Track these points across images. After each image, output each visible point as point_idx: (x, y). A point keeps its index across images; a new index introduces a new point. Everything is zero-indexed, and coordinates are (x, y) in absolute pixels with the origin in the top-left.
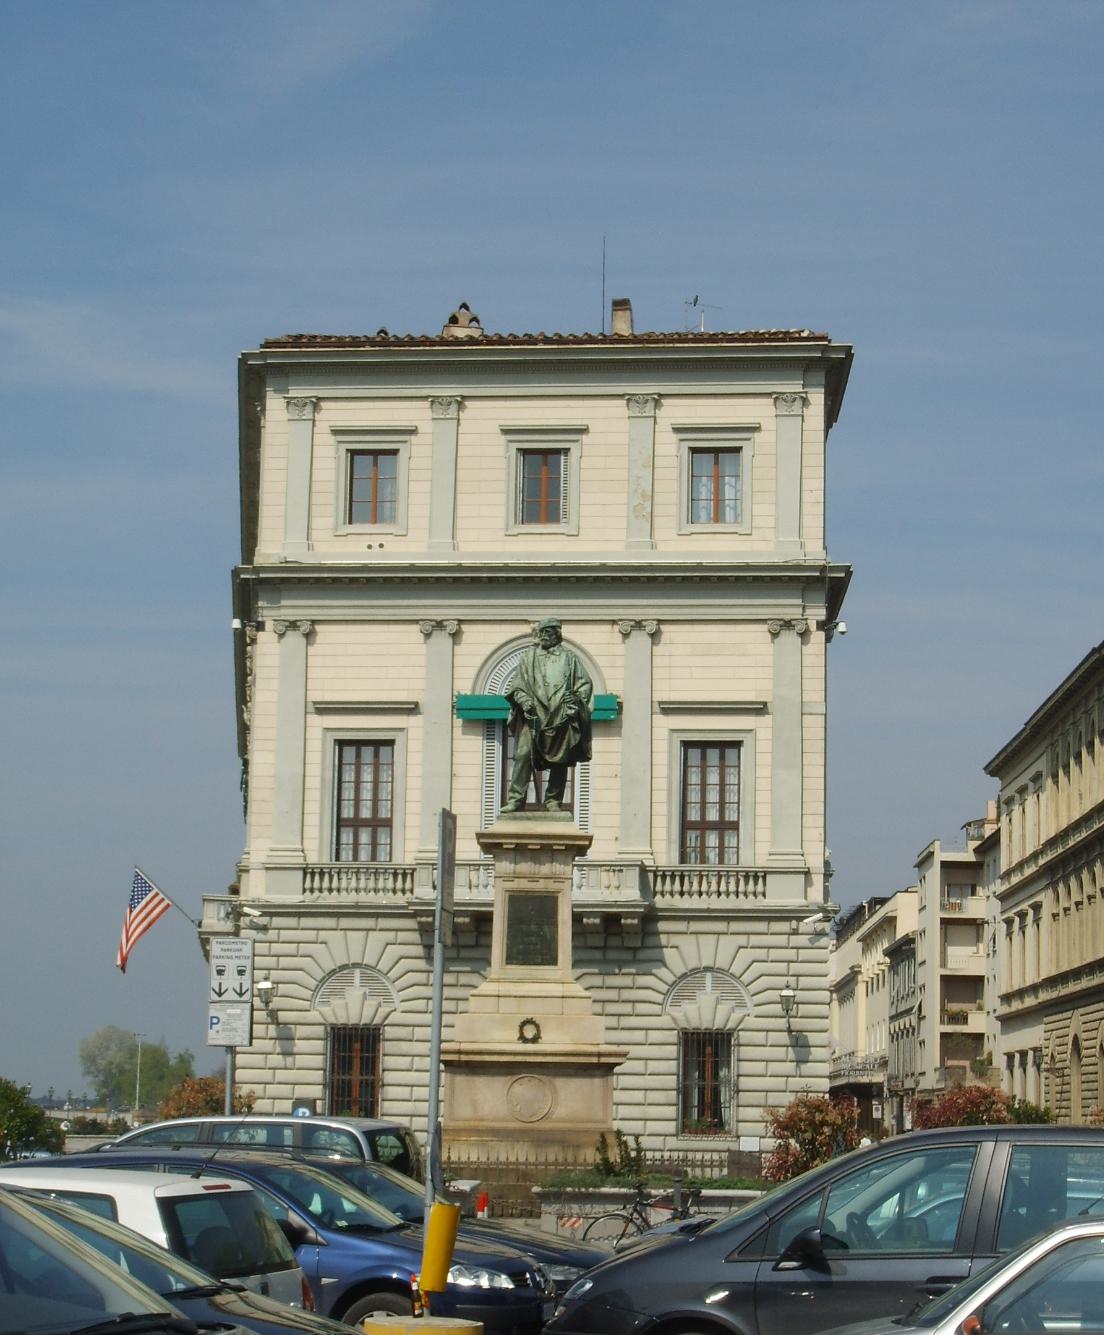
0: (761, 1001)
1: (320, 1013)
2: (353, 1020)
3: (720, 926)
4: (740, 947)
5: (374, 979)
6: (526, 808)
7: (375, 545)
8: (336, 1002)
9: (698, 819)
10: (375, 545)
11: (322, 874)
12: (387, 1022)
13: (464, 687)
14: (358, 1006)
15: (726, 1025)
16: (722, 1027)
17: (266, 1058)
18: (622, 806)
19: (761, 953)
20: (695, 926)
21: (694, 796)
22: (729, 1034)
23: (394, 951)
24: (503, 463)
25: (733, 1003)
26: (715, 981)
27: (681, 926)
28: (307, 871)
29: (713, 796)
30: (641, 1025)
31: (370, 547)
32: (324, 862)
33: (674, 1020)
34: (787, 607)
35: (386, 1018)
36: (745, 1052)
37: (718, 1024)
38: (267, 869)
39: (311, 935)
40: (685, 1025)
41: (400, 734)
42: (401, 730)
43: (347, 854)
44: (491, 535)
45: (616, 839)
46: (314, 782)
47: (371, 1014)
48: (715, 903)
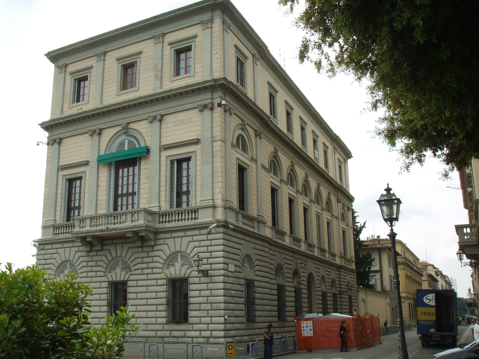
2: (178, 276)
3: (182, 234)
4: (190, 242)
10: (80, 109)
16: (183, 276)
18: (151, 187)
19: (197, 244)
20: (174, 235)
25: (188, 266)
27: (168, 235)
34: (205, 98)
37: (182, 275)
40: (170, 277)
42: (84, 172)
44: (113, 96)
48: (180, 224)
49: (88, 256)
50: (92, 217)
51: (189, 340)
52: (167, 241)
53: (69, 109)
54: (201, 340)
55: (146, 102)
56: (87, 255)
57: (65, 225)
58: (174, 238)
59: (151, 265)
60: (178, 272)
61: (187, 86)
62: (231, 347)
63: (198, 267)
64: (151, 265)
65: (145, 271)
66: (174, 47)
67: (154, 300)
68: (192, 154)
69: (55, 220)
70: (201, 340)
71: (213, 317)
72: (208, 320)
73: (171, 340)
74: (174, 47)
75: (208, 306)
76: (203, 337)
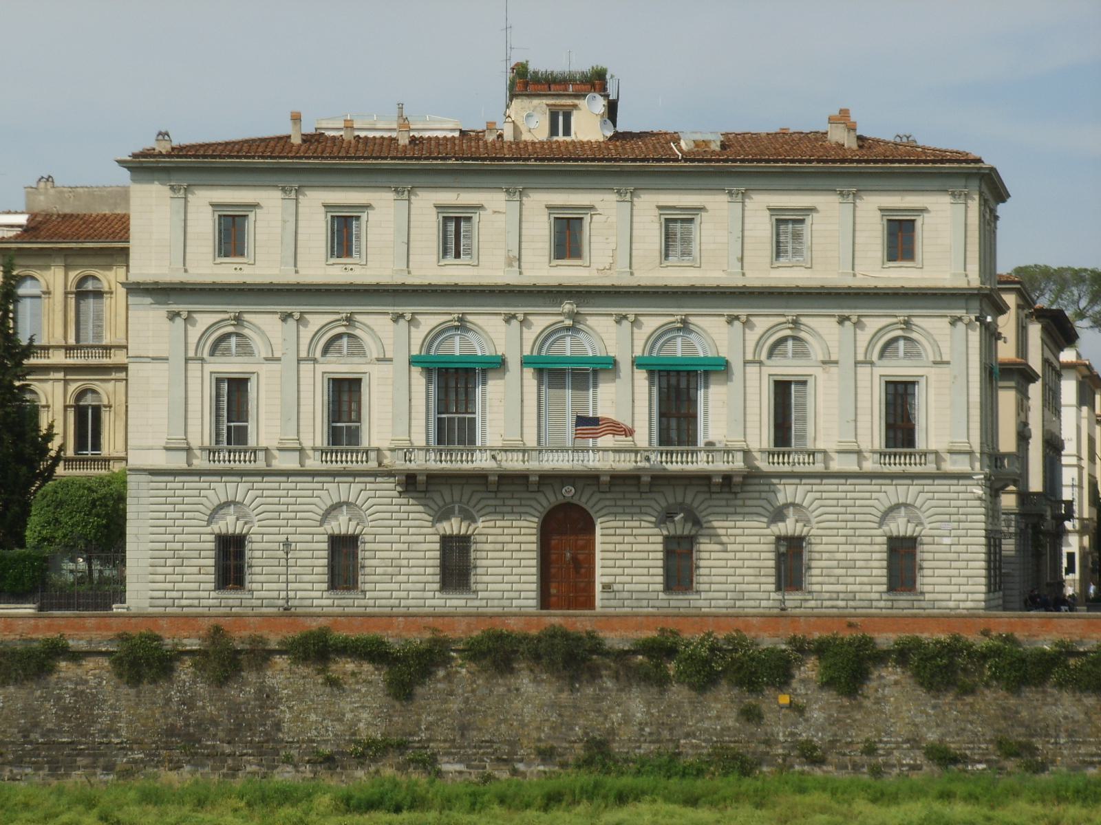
6: (664, 419)
14: (904, 527)
19: (818, 495)
22: (469, 537)
24: (547, 226)
36: (926, 548)
46: (194, 405)
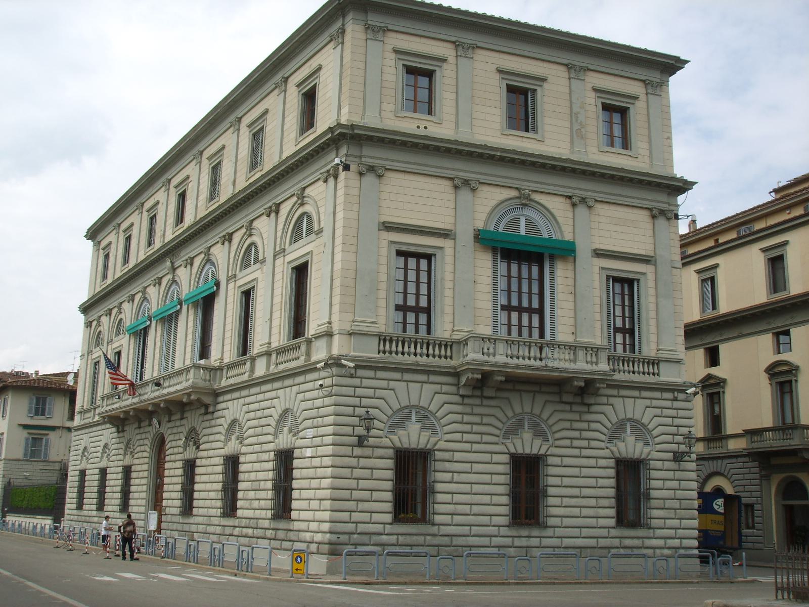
0: (659, 442)
1: (390, 439)
2: (413, 446)
5: (426, 417)
7: (422, 127)
8: (401, 432)
9: (528, 306)
10: (422, 127)
11: (391, 341)
12: (436, 447)
13: (480, 225)
15: (641, 456)
16: (639, 457)
17: (352, 471)
18: (576, 310)
21: (424, 278)
23: (440, 399)
26: (632, 427)
28: (383, 339)
29: (412, 276)
30: (594, 455)
31: (426, 128)
32: (390, 332)
33: (612, 452)
35: (435, 444)
37: (421, 446)
38: (350, 334)
39: (384, 384)
41: (439, 251)
43: (411, 329)
45: (573, 333)
47: (425, 441)
49: (462, 404)
50: (521, 341)
51: (649, 552)
52: (612, 400)
53: (395, 118)
54: (666, 552)
55: (631, 180)
56: (461, 402)
57: (626, 358)
58: (623, 397)
59: (586, 434)
60: (414, 439)
61: (622, 170)
62: (299, 559)
63: (690, 448)
64: (586, 434)
65: (576, 443)
66: (604, 98)
67: (487, 486)
68: (437, 250)
69: (330, 324)
70: (666, 552)
71: (683, 519)
72: (675, 523)
73: (622, 551)
74: (604, 98)
75: (676, 504)
76: (669, 548)
